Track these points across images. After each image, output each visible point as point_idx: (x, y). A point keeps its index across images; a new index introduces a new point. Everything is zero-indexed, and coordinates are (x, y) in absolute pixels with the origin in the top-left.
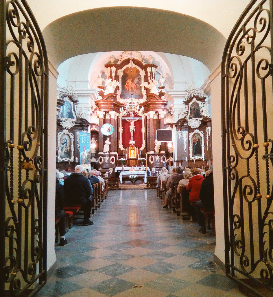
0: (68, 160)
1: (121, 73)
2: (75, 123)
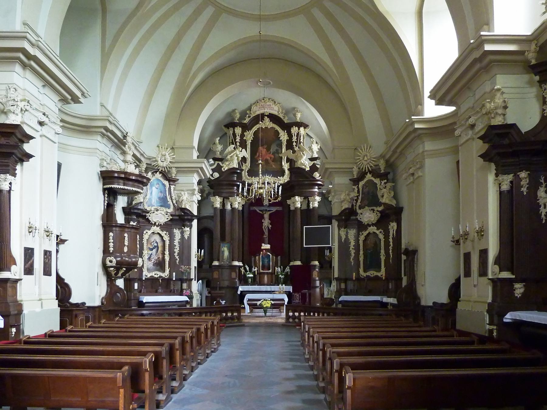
0: (159, 276)
1: (249, 136)
2: (171, 215)
